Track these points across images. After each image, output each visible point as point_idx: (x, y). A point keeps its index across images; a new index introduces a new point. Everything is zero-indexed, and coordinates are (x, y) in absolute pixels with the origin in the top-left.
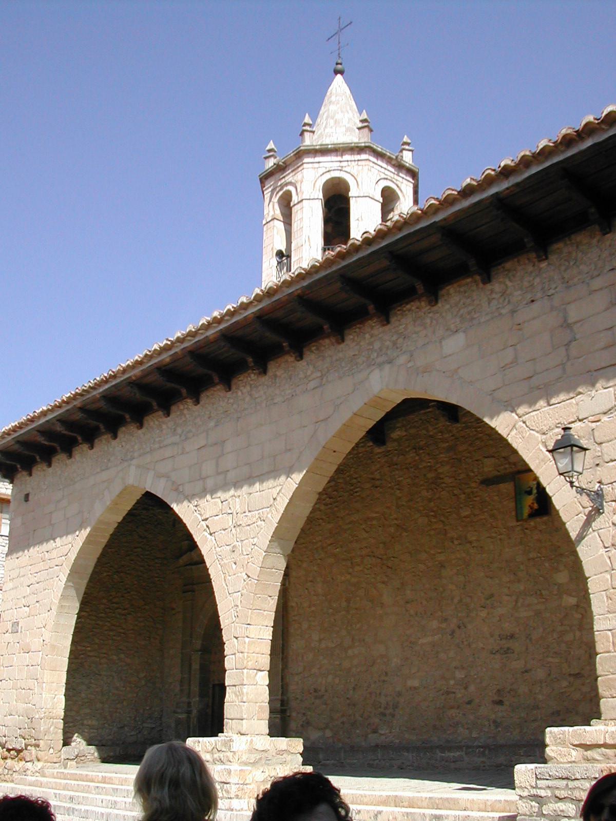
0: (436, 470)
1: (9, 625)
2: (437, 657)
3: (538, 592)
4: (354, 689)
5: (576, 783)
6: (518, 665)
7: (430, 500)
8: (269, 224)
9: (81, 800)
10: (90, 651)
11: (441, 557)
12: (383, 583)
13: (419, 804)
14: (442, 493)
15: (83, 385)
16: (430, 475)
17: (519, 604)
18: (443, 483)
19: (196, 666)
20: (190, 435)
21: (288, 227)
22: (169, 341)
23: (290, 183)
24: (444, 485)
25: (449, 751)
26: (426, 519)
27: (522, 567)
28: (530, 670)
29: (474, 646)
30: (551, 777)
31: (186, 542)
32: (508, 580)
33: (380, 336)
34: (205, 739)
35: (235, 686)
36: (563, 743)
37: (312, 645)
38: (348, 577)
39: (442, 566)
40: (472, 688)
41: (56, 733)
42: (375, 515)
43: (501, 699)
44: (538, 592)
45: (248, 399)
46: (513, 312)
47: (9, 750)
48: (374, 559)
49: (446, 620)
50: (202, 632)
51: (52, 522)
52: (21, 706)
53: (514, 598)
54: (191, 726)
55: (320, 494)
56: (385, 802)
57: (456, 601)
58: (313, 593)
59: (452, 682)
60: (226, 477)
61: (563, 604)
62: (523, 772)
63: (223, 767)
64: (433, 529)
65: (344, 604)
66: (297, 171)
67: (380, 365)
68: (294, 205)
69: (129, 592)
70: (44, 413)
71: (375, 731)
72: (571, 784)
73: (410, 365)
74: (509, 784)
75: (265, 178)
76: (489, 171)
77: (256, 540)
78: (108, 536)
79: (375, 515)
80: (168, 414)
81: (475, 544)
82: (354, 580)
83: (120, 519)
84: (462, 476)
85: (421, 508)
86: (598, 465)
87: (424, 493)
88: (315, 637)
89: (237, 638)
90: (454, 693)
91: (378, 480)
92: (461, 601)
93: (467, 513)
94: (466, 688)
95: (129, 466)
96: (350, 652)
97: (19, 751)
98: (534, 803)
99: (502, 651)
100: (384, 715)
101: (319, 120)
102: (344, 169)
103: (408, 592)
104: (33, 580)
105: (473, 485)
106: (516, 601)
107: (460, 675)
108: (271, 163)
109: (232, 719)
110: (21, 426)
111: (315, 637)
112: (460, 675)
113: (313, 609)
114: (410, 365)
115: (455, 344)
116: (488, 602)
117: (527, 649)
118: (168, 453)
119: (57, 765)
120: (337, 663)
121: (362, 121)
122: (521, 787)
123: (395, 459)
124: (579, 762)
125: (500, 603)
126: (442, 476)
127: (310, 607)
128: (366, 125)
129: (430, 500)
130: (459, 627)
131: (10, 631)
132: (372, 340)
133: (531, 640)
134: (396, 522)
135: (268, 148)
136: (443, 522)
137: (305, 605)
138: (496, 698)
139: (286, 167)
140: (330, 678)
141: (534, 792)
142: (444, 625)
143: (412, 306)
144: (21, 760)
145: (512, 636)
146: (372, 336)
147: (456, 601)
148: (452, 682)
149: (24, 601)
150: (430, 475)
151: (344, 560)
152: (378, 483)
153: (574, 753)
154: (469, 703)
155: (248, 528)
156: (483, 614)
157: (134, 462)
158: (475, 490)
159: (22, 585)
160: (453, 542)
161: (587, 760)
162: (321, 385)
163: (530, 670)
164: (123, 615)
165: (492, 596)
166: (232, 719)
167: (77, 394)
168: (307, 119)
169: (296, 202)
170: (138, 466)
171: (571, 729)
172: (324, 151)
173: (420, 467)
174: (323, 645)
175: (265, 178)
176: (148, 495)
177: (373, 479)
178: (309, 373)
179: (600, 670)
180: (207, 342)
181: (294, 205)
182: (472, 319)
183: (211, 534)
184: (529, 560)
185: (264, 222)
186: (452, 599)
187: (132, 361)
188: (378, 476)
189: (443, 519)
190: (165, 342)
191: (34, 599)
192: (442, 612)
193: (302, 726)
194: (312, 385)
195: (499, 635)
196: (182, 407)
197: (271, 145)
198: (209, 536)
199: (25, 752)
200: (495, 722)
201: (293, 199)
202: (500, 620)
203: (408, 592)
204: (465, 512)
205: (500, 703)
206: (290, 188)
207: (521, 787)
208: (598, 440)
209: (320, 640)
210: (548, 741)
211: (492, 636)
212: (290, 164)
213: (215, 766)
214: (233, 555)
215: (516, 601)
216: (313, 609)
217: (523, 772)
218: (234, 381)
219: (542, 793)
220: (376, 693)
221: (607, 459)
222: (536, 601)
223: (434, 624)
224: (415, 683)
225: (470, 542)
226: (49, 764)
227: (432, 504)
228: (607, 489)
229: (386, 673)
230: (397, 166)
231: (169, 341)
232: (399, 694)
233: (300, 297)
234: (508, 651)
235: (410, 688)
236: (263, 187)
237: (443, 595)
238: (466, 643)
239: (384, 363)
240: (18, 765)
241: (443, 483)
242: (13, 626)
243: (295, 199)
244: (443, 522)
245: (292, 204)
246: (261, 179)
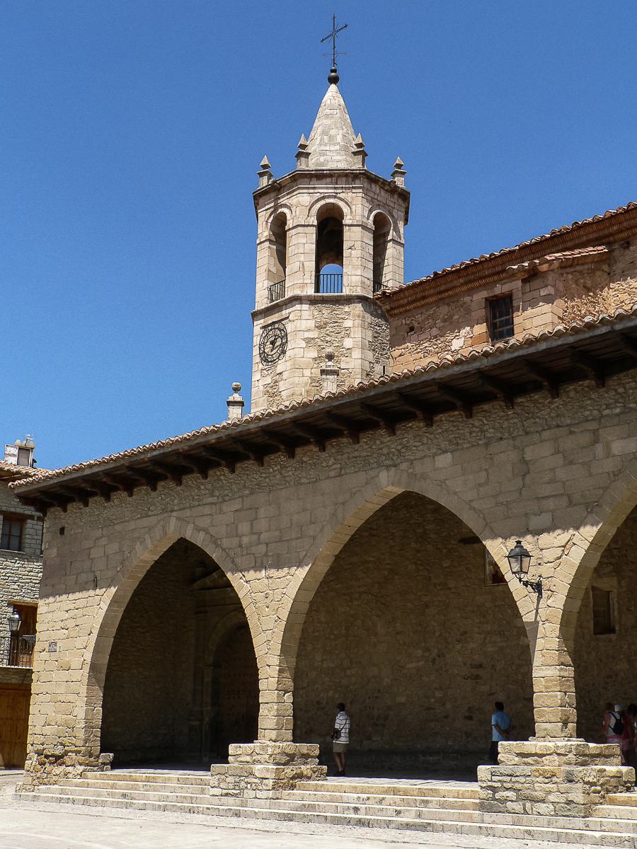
0: (424, 526)
1: (46, 646)
2: (421, 680)
3: (502, 633)
4: (351, 703)
5: (517, 779)
6: (485, 688)
7: (418, 551)
8: (263, 244)
9: (134, 796)
10: (114, 666)
11: (426, 599)
12: (378, 616)
13: (412, 793)
14: (428, 546)
15: (133, 450)
16: (419, 531)
17: (487, 641)
18: (429, 538)
19: (208, 679)
20: (227, 498)
21: (281, 247)
22: (216, 427)
23: (285, 206)
24: (429, 540)
25: (431, 756)
26: (414, 566)
27: (490, 611)
28: (494, 693)
29: (450, 672)
30: (502, 775)
31: (200, 568)
32: (478, 621)
33: (388, 444)
34: (246, 745)
35: (268, 703)
36: (509, 752)
37: (316, 665)
38: (348, 609)
39: (427, 606)
40: (448, 706)
41: (95, 740)
42: (371, 559)
43: (471, 715)
44: (502, 633)
45: (278, 476)
46: (487, 445)
47: (47, 757)
48: (370, 596)
49: (429, 650)
50: (215, 649)
51: (91, 557)
52: (60, 718)
53: (483, 636)
54: (203, 731)
55: (336, 556)
56: (387, 791)
57: (437, 634)
58: (316, 621)
59: (432, 700)
60: (259, 538)
61: (521, 643)
62: (483, 770)
63: (262, 766)
64: (420, 575)
65: (344, 631)
66: (292, 194)
67: (388, 467)
68: (289, 230)
69: (147, 612)
70: (90, 466)
71: (369, 738)
72: (514, 779)
73: (410, 471)
74: (472, 777)
75: (259, 196)
76: (474, 352)
77: (285, 590)
78: (145, 571)
79: (371, 559)
80: (206, 477)
81: (453, 591)
82: (352, 612)
83: (157, 558)
84: (444, 534)
85: (411, 557)
86: (540, 564)
87: (413, 545)
88: (318, 658)
89: (269, 666)
90: (434, 709)
91: (374, 530)
92: (440, 635)
93: (447, 565)
94: (444, 705)
95: (170, 517)
96: (348, 672)
97: (58, 758)
98: (490, 792)
99: (473, 678)
100: (376, 725)
101: (312, 134)
102: (339, 195)
103: (398, 624)
104: (72, 607)
105: (453, 542)
106: (485, 639)
107: (438, 694)
108: (264, 182)
109: (265, 729)
110: (65, 473)
111: (318, 658)
112: (438, 694)
113: (317, 634)
114: (410, 471)
115: (444, 460)
116: (462, 637)
117: (492, 677)
118: (207, 510)
119: (96, 768)
120: (338, 680)
121: (359, 145)
122: (481, 781)
123: (390, 513)
124: (520, 765)
125: (472, 639)
126: (428, 532)
127: (313, 632)
128: (361, 152)
129: (418, 551)
130: (439, 656)
131: (47, 650)
132: (382, 446)
133: (495, 669)
134: (388, 566)
135: (262, 163)
136: (428, 570)
137: (310, 630)
138: (467, 714)
139: (281, 187)
140: (331, 693)
141: (490, 784)
142: (427, 654)
143: (413, 425)
144: (60, 765)
145: (480, 666)
146: (382, 443)
147: (437, 634)
148: (432, 700)
149: (62, 625)
150: (419, 531)
151: (345, 594)
152: (375, 532)
153: (517, 759)
154: (446, 717)
155: (279, 580)
156: (458, 647)
157: (174, 514)
158: (455, 546)
159: (59, 609)
160: (435, 587)
161: (526, 764)
162: (340, 475)
163: (494, 693)
164: (143, 633)
165: (466, 633)
166: (265, 729)
167: (125, 455)
168: (302, 141)
169: (291, 226)
170: (178, 518)
171: (515, 743)
172: (319, 176)
173: (411, 522)
174: (325, 666)
175: (259, 196)
176: (182, 541)
177: (371, 528)
178: (331, 463)
179: (535, 704)
180: (249, 433)
181: (289, 230)
182: (457, 444)
183: (247, 582)
184: (496, 606)
185: (258, 242)
186: (434, 634)
187: (181, 437)
188: (375, 527)
189: (428, 568)
190: (212, 428)
191: (71, 624)
192: (425, 643)
193: (306, 733)
194: (332, 474)
195: (471, 665)
196: (218, 473)
197: (265, 161)
198: (244, 583)
199: (65, 757)
200: (466, 733)
201: (288, 222)
202: (471, 653)
203: (398, 624)
204: (446, 564)
205: (470, 718)
206: (285, 210)
207: (481, 781)
208: (541, 547)
209: (322, 661)
210: (499, 750)
211: (465, 665)
212: (285, 186)
213: (255, 766)
214: (266, 600)
215: (485, 639)
216: (317, 634)
217: (483, 770)
218: (266, 459)
219: (496, 785)
220: (370, 707)
221: (546, 561)
222: (499, 640)
223: (419, 652)
224: (402, 699)
225: (450, 589)
226: (89, 768)
227: (419, 555)
228: (544, 582)
229: (379, 691)
230: (389, 192)
231: (216, 427)
232: (389, 708)
233: (328, 412)
234: (477, 677)
235: (398, 703)
236: (256, 207)
237: (427, 629)
238: (444, 670)
239: (390, 466)
240: (58, 770)
241: (429, 538)
242: (50, 646)
243: (290, 224)
244: (428, 570)
245: (287, 228)
246: (254, 197)
